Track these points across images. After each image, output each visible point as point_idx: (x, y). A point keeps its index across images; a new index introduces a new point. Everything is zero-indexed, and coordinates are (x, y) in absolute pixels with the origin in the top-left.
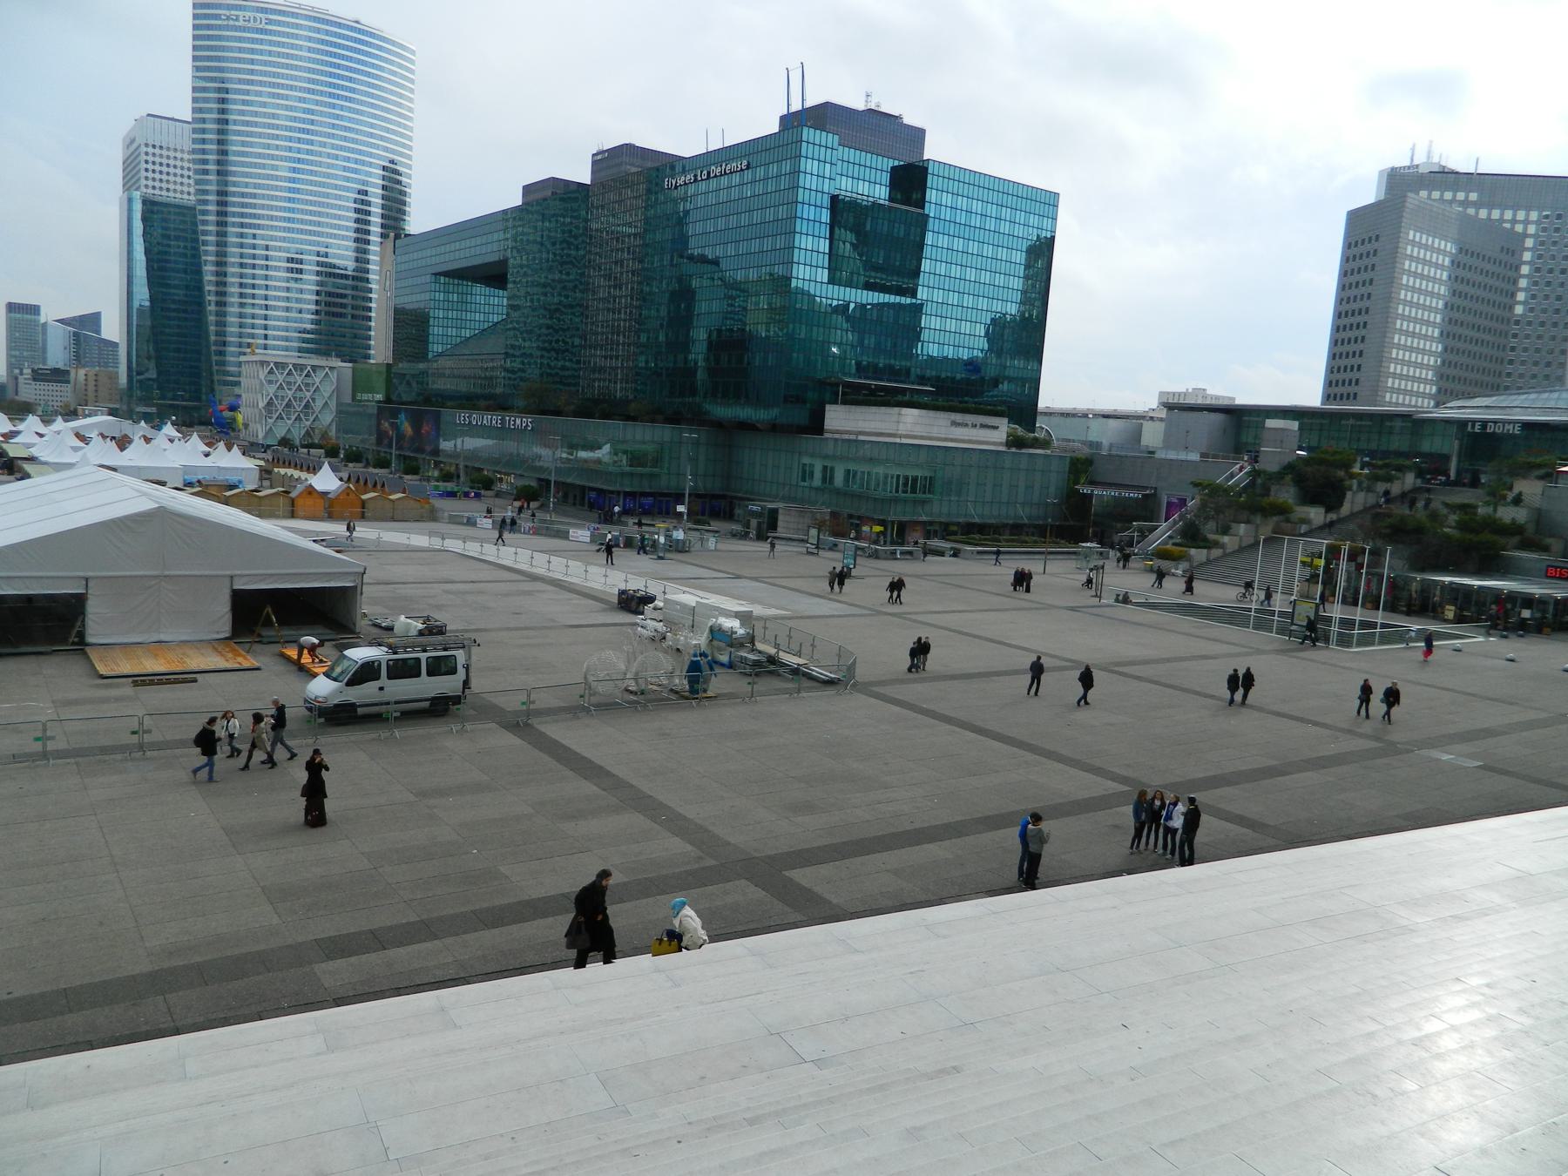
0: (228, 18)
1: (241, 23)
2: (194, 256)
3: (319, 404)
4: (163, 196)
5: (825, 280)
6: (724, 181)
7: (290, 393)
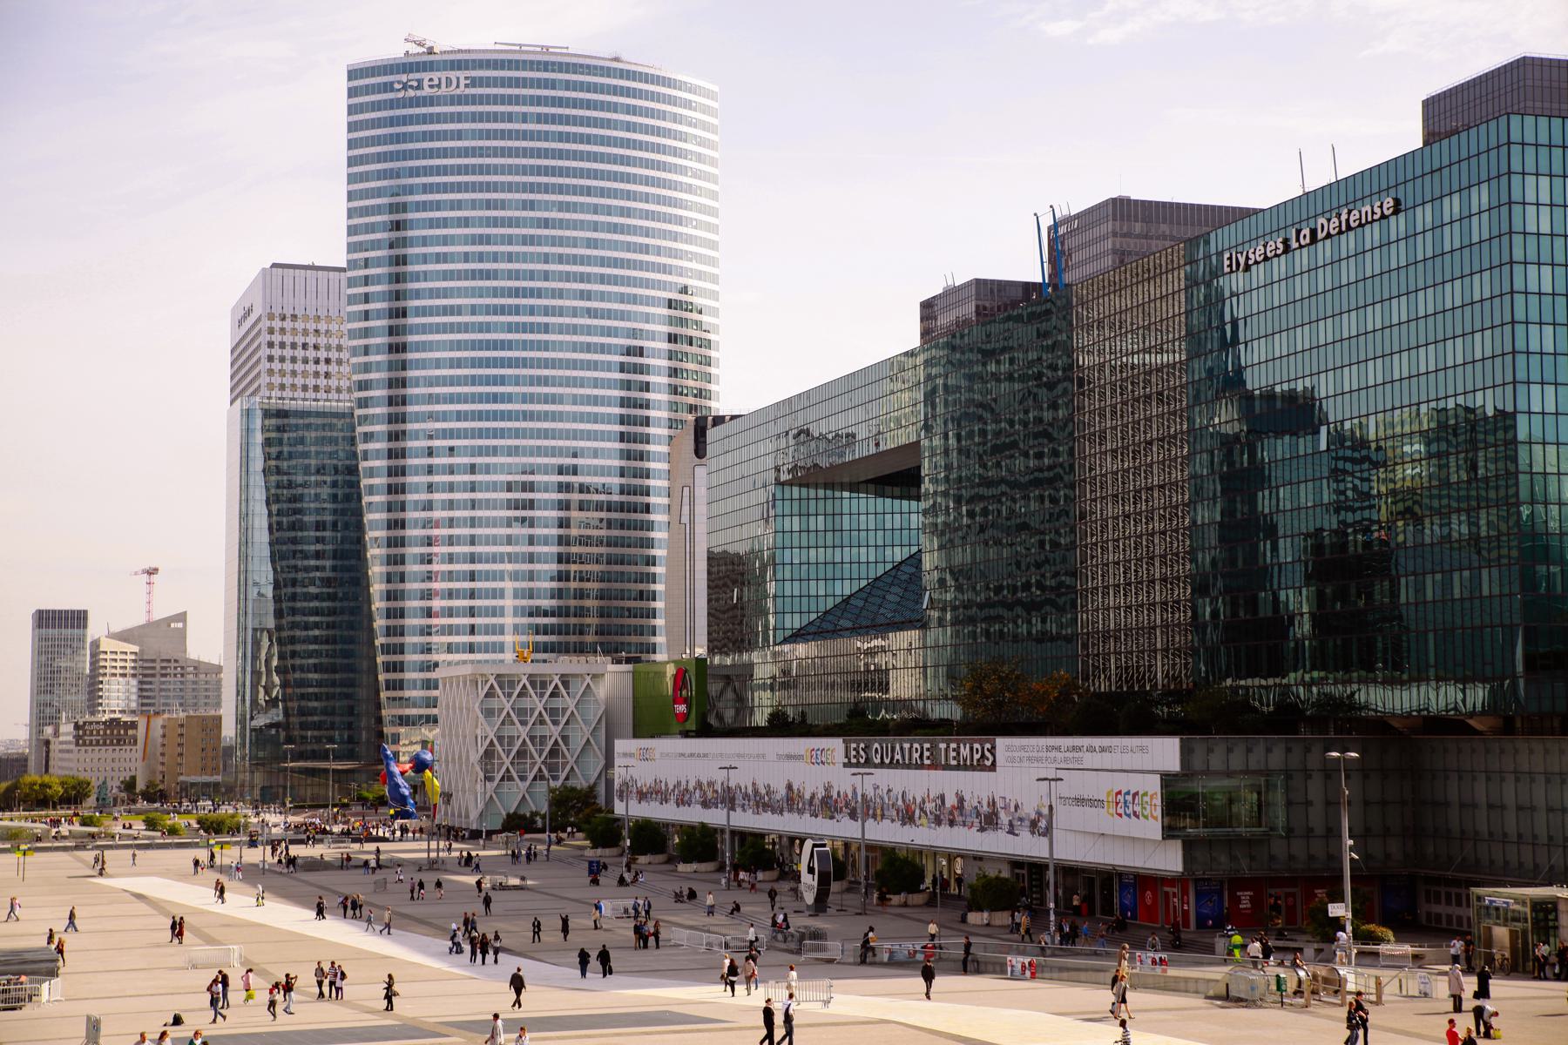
0: (405, 87)
1: (427, 91)
2: (347, 498)
3: (578, 742)
4: (298, 402)
5: (1522, 421)
6: (1349, 242)
7: (523, 732)
